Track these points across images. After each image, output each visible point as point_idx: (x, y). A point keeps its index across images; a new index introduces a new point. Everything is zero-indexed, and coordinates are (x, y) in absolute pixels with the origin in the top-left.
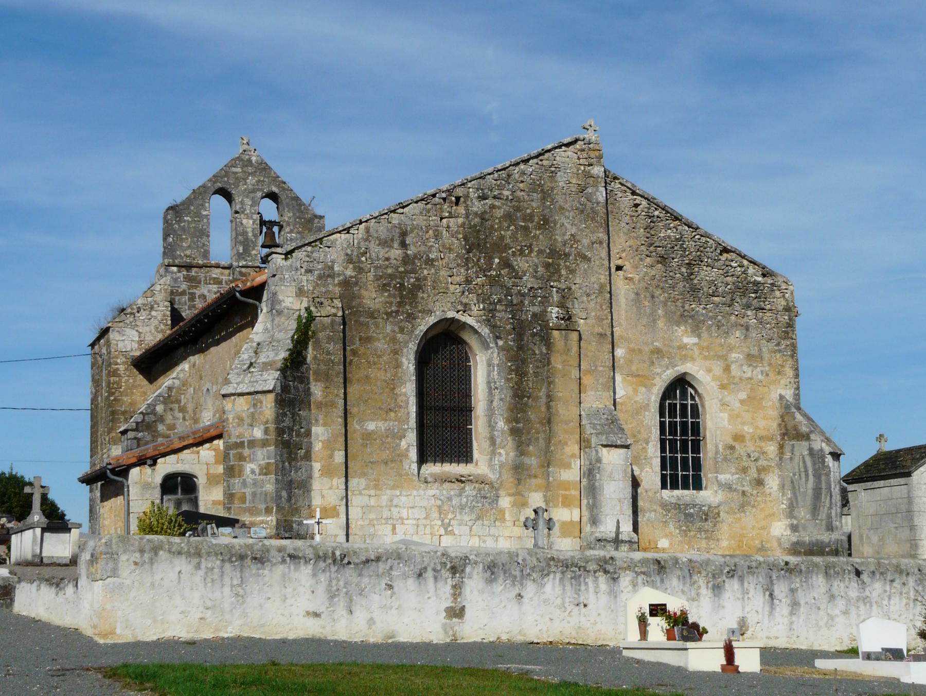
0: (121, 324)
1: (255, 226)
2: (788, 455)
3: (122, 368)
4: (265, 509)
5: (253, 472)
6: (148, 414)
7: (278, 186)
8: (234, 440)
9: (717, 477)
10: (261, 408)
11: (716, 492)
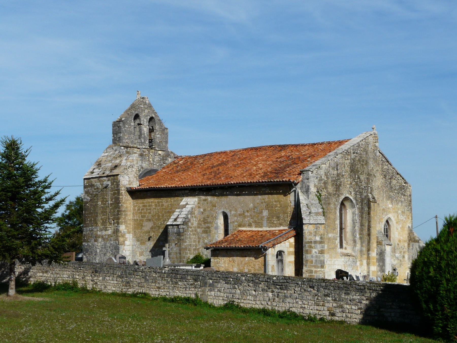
0: (123, 173)
1: (147, 131)
2: (411, 248)
3: (123, 192)
4: (321, 266)
5: (316, 252)
6: (186, 218)
7: (155, 115)
8: (308, 240)
9: (395, 255)
10: (319, 229)
11: (395, 260)
